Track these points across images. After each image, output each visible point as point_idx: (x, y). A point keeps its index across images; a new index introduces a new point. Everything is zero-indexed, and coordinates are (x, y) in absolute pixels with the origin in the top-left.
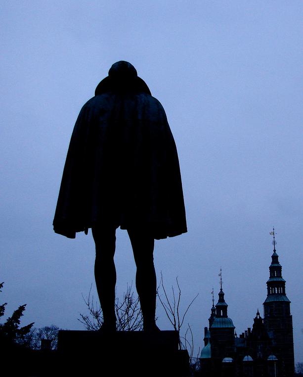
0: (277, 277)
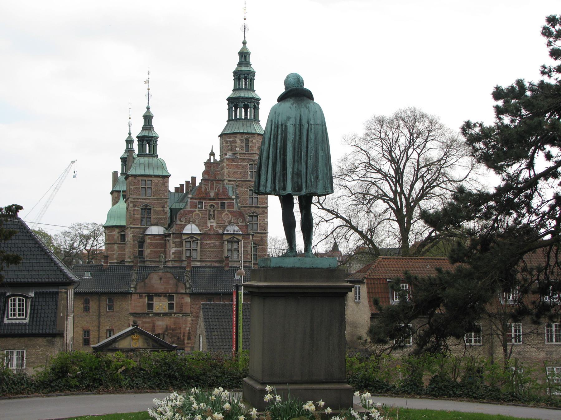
0: (246, 89)
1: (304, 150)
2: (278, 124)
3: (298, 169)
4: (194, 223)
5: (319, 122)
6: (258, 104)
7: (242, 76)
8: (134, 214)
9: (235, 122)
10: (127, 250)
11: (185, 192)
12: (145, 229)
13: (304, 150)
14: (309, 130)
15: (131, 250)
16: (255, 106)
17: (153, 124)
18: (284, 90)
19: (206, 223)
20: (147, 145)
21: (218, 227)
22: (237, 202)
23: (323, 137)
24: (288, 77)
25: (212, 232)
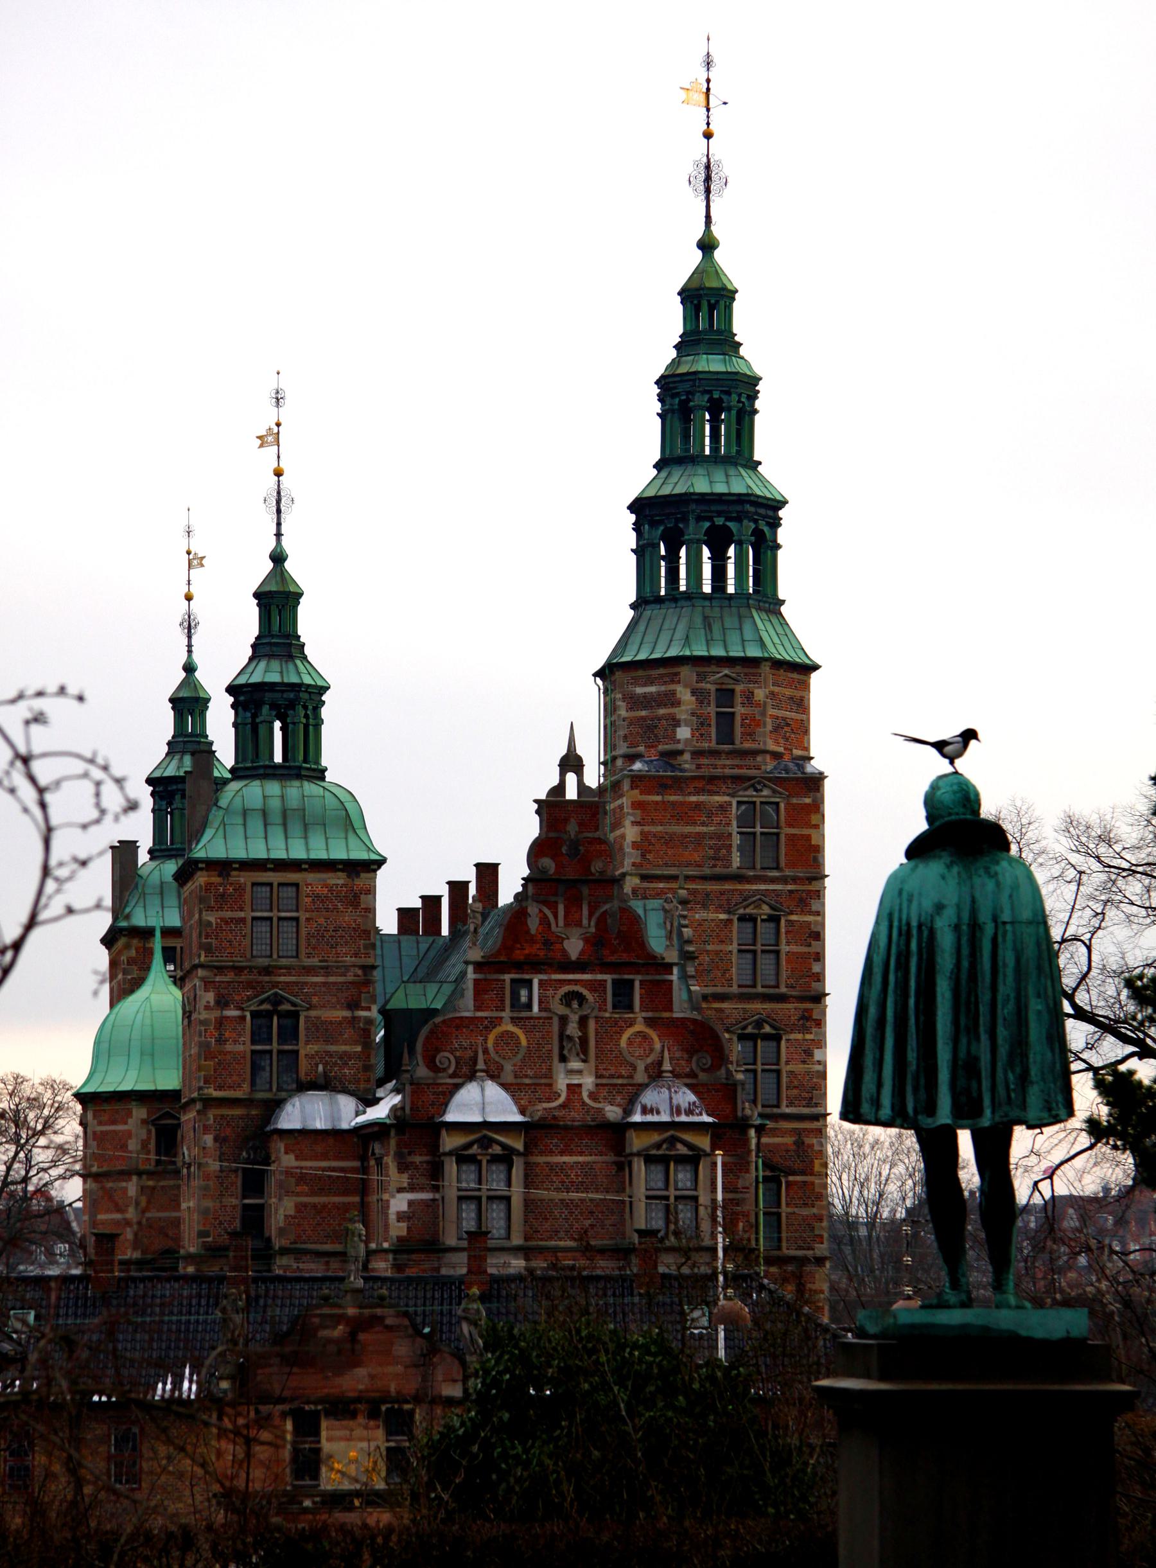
0: (716, 459)
1: (985, 997)
2: (908, 924)
3: (969, 1052)
4: (493, 1077)
5: (1026, 914)
6: (776, 523)
7: (700, 400)
8: (221, 1041)
9: (670, 613)
10: (188, 1204)
11: (445, 931)
12: (275, 1106)
13: (985, 997)
14: (1000, 939)
15: (209, 1203)
16: (759, 535)
17: (301, 631)
18: (923, 826)
19: (549, 1074)
20: (277, 725)
21: (604, 1093)
22: (684, 977)
23: (1039, 957)
24: (934, 787)
25: (575, 1116)
